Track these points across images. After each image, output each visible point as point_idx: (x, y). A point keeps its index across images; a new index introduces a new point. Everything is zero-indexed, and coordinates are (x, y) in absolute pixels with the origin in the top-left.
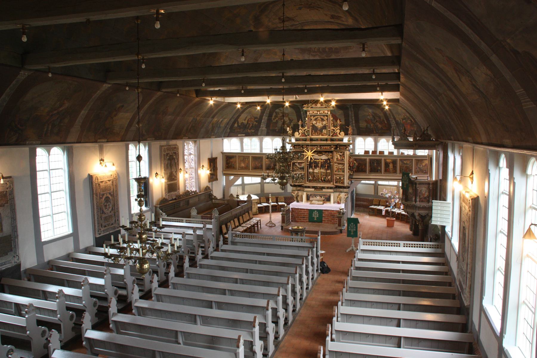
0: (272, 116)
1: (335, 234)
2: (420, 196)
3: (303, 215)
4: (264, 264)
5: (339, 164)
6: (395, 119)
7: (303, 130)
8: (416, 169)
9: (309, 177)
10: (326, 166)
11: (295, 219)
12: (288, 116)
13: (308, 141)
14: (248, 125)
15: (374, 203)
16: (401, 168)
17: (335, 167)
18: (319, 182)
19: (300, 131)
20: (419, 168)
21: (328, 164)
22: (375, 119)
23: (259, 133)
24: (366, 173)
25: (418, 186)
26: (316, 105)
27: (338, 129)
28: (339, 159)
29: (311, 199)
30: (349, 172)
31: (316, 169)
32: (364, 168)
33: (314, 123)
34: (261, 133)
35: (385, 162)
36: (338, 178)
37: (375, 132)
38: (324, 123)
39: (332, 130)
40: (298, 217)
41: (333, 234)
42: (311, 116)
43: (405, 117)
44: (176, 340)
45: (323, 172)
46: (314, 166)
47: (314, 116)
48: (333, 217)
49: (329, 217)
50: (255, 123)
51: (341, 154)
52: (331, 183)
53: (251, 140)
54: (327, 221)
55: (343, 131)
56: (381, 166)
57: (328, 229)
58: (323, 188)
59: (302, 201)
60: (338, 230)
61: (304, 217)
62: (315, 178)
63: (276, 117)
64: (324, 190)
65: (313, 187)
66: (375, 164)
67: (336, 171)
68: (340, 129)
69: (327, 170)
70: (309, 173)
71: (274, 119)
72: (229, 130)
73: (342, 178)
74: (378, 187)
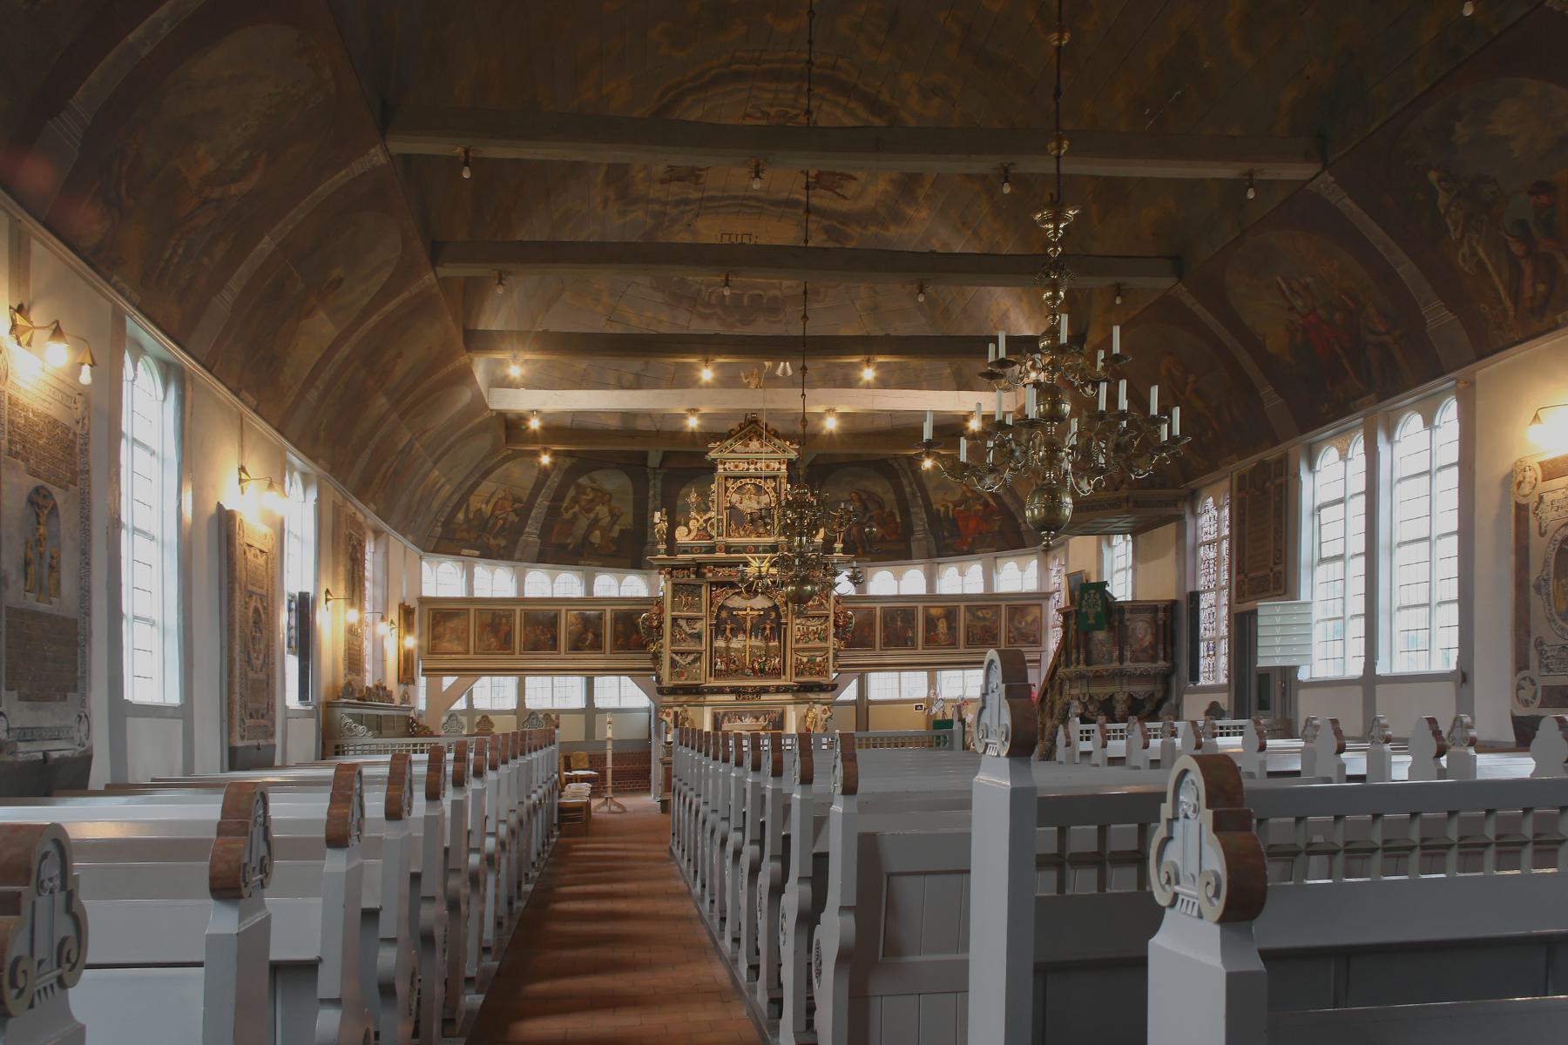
0: (562, 500)
2: (1131, 646)
6: (928, 505)
7: (701, 521)
8: (1010, 632)
9: (716, 664)
10: (768, 626)
12: (610, 500)
13: (720, 551)
14: (491, 522)
16: (968, 632)
19: (692, 524)
20: (1017, 629)
23: (517, 555)
24: (874, 650)
25: (1127, 616)
26: (747, 446)
31: (735, 639)
32: (866, 634)
33: (733, 500)
35: (927, 618)
36: (805, 660)
38: (765, 499)
42: (726, 478)
43: (969, 494)
45: (757, 647)
46: (732, 629)
47: (736, 478)
52: (783, 677)
53: (493, 574)
56: (914, 628)
58: (765, 690)
63: (575, 501)
64: (764, 697)
65: (735, 691)
66: (899, 623)
67: (797, 641)
69: (767, 639)
71: (567, 509)
72: (440, 529)
74: (868, 708)
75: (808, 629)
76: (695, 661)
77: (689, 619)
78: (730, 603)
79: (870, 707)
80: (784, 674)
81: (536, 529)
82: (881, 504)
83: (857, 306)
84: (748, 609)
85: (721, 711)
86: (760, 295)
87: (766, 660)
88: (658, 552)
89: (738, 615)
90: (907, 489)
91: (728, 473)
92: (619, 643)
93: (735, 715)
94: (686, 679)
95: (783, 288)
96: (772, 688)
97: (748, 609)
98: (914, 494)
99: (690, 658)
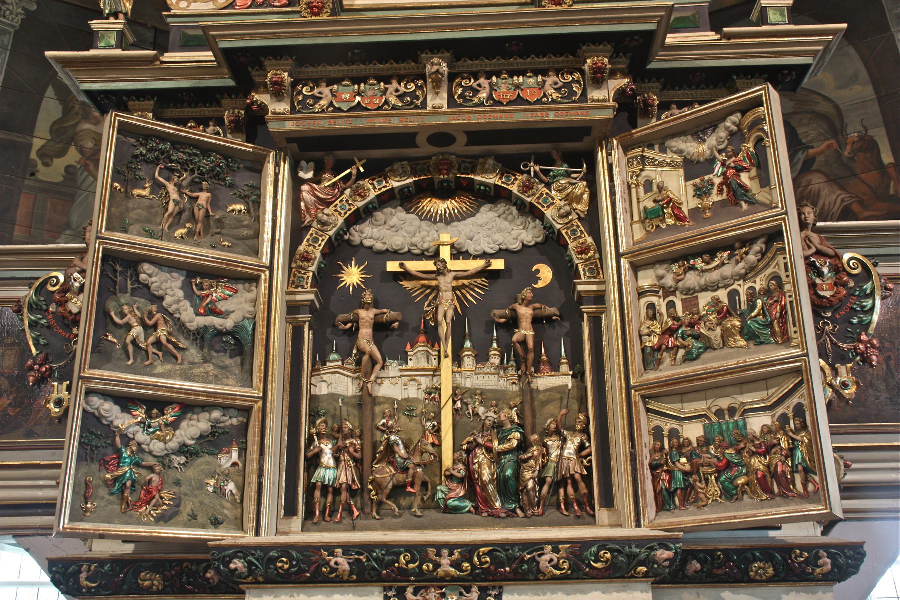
4: (640, 421)
9: (314, 462)
10: (525, 312)
31: (394, 369)
36: (693, 432)
44: (726, 412)
45: (485, 396)
46: (380, 328)
52: (602, 515)
62: (386, 473)
70: (314, 415)
71: (46, 156)
75: (691, 304)
80: (608, 502)
84: (445, 253)
87: (524, 445)
89: (407, 275)
94: (164, 519)
97: (445, 253)
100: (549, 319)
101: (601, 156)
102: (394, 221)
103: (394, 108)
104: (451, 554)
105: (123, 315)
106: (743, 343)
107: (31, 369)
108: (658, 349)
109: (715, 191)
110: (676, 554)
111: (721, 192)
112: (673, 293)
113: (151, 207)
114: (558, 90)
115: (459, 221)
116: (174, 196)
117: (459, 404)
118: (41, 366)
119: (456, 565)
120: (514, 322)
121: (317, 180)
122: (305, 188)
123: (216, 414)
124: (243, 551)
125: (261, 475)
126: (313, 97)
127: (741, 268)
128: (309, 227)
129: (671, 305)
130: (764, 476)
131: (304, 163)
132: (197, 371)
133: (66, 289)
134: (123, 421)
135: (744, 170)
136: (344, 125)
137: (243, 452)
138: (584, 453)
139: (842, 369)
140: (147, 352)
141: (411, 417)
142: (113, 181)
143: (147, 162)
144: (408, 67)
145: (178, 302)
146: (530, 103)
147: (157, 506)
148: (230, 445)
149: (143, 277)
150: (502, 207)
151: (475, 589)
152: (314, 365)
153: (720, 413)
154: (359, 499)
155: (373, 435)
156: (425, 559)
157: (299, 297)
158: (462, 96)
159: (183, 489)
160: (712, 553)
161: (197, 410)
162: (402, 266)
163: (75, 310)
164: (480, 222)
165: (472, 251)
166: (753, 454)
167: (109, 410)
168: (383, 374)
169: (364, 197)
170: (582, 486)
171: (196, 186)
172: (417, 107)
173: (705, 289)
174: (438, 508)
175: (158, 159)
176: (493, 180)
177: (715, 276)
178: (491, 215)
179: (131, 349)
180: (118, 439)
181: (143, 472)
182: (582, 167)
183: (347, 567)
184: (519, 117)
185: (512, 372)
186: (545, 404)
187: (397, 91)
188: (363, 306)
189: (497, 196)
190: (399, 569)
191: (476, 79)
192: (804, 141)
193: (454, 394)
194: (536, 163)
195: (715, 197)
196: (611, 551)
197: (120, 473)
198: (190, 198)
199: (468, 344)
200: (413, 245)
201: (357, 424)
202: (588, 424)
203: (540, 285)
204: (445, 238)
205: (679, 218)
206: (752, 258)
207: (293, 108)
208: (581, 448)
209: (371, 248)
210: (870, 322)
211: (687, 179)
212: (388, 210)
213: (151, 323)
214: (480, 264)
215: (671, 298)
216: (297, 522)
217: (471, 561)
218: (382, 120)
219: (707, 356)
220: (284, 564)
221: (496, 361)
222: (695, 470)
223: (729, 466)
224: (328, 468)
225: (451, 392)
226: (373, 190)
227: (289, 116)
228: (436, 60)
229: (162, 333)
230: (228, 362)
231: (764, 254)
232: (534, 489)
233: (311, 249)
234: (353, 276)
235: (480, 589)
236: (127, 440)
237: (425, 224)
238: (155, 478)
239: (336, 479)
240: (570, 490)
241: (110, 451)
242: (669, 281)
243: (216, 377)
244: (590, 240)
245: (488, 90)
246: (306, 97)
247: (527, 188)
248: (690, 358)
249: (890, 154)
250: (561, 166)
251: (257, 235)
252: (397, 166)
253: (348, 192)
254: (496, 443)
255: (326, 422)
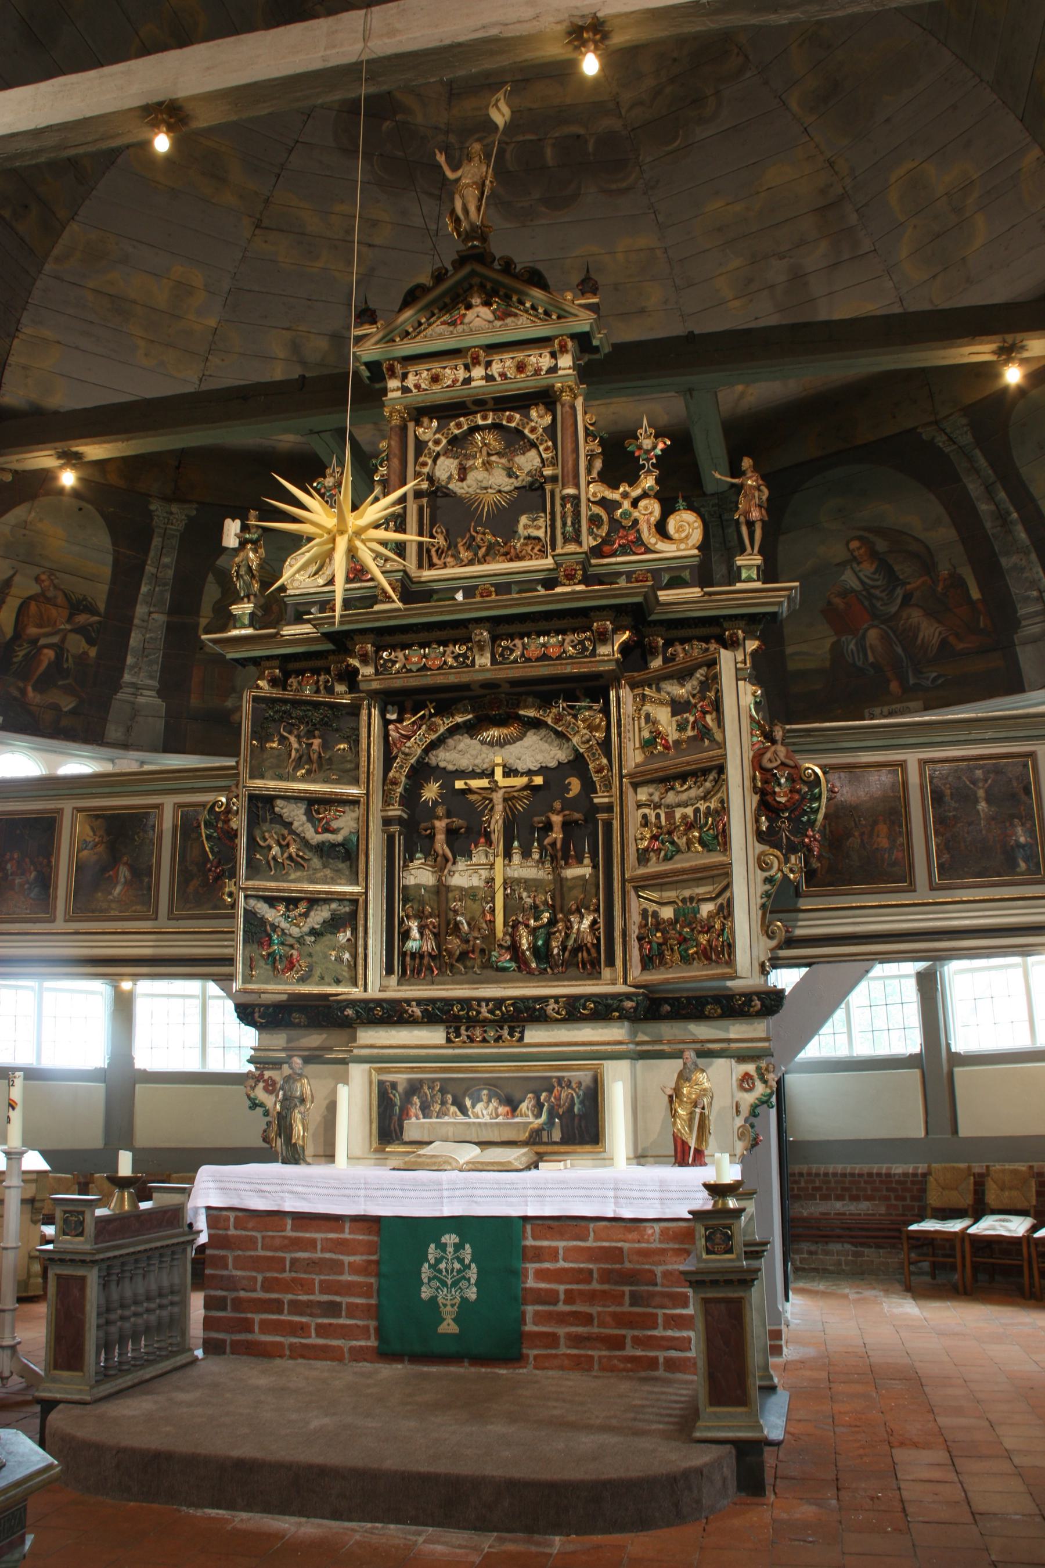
0: (195, 610)
1: (678, 1516)
3: (326, 1287)
5: (666, 780)
9: (406, 935)
10: (556, 819)
11: (246, 1326)
15: (934, 1198)
17: (634, 817)
18: (496, 973)
21: (568, 805)
22: (893, 580)
23: (113, 732)
24: (912, 889)
27: (645, 495)
28: (673, 735)
29: (415, 1126)
30: (762, 864)
31: (462, 864)
34: (129, 730)
36: (667, 913)
37: (894, 686)
38: (528, 462)
39: (597, 510)
40: (276, 1306)
41: (643, 1523)
45: (528, 884)
46: (451, 833)
48: (636, 1299)
49: (592, 1297)
50: (77, 644)
51: (681, 691)
52: (606, 973)
54: (577, 1340)
55: (690, 508)
57: (587, 1442)
59: (330, 1157)
60: (701, 1457)
61: (333, 1309)
62: (454, 943)
64: (535, 1035)
66: (982, 806)
67: (643, 856)
68: (658, 496)
73: (706, 909)
74: (951, 1075)
75: (670, 816)
76: (334, 924)
77: (314, 803)
78: (446, 758)
79: (957, 1070)
80: (611, 963)
81: (151, 677)
82: (926, 562)
83: (794, 105)
84: (499, 772)
85: (401, 1079)
86: (579, 136)
87: (553, 922)
88: (232, 621)
89: (469, 791)
90: (984, 508)
91: (416, 398)
92: (191, 889)
93: (443, 1091)
94: (302, 980)
95: (623, 112)
96: (552, 1006)
97: (499, 772)
98: (1002, 517)
99: (319, 916)
100: (576, 822)
101: (613, 694)
102: (461, 746)
103: (451, 667)
104: (487, 1005)
105: (265, 840)
106: (700, 849)
107: (210, 870)
108: (646, 850)
109: (689, 727)
110: (637, 1004)
111: (693, 728)
112: (659, 807)
113: (280, 755)
114: (574, 647)
115: (510, 744)
116: (295, 745)
117: (509, 891)
118: (216, 868)
119: (490, 1012)
120: (548, 827)
121: (400, 720)
122: (391, 727)
123: (334, 906)
124: (353, 1003)
125: (366, 948)
126: (390, 660)
127: (701, 792)
128: (396, 757)
129: (658, 816)
130: (705, 948)
131: (390, 707)
132: (319, 875)
133: (228, 811)
134: (272, 915)
135: (707, 712)
136: (413, 682)
137: (354, 931)
138: (596, 927)
139: (793, 858)
140: (283, 864)
141: (474, 900)
142: (252, 740)
143: (274, 720)
144: (460, 633)
145: (303, 825)
146: (553, 659)
147: (297, 972)
148: (344, 927)
149: (277, 809)
150: (543, 732)
151: (506, 1027)
152: (404, 862)
153: (684, 900)
154: (438, 961)
155: (447, 914)
156: (470, 1008)
157: (390, 813)
158: (502, 655)
159: (314, 959)
160: (678, 999)
161: (321, 903)
162: (466, 784)
163: (235, 827)
164: (526, 745)
165: (520, 769)
166: (700, 932)
167: (263, 909)
168: (454, 868)
169: (436, 732)
170: (593, 951)
171: (310, 734)
172: (468, 666)
173: (679, 805)
174: (492, 967)
175: (282, 717)
176: (531, 713)
177: (684, 797)
178: (535, 738)
179: (272, 863)
180: (268, 928)
181: (287, 948)
182: (599, 702)
183: (419, 1014)
184: (544, 670)
185: (547, 865)
186: (571, 889)
187: (453, 653)
188: (439, 818)
189: (536, 724)
190: (454, 1015)
191: (512, 640)
192: (901, 577)
193: (505, 882)
194: (564, 701)
195: (690, 733)
196: (594, 1002)
197: (271, 950)
198: (307, 744)
199: (516, 844)
200: (475, 765)
201: (435, 907)
202: (599, 906)
203: (571, 794)
204: (499, 760)
205: (666, 747)
206: (708, 785)
207: (377, 670)
208: (594, 922)
209: (444, 769)
210: (815, 820)
211: (673, 714)
212: (457, 737)
213: (284, 843)
214: (525, 780)
215: (658, 811)
216: (394, 979)
217: (501, 1010)
218: (442, 677)
219: (677, 857)
220: (378, 1011)
221: (536, 856)
222: (665, 943)
223: (685, 940)
224: (415, 940)
225: (502, 881)
226: (443, 725)
227: (374, 677)
228: (477, 631)
229: (292, 849)
230: (341, 866)
231: (716, 781)
232: (558, 954)
233: (397, 775)
234: (431, 792)
235: (509, 1027)
236: (274, 927)
237: (485, 748)
238: (295, 953)
239: (421, 947)
240: (585, 954)
241: (263, 935)
242: (656, 798)
243: (332, 878)
244: (605, 761)
245: (521, 649)
246: (385, 660)
247: (558, 719)
248: (668, 858)
249: (977, 590)
250: (584, 701)
251: (357, 767)
252: (460, 706)
253: (424, 727)
254: (532, 921)
255: (412, 907)
